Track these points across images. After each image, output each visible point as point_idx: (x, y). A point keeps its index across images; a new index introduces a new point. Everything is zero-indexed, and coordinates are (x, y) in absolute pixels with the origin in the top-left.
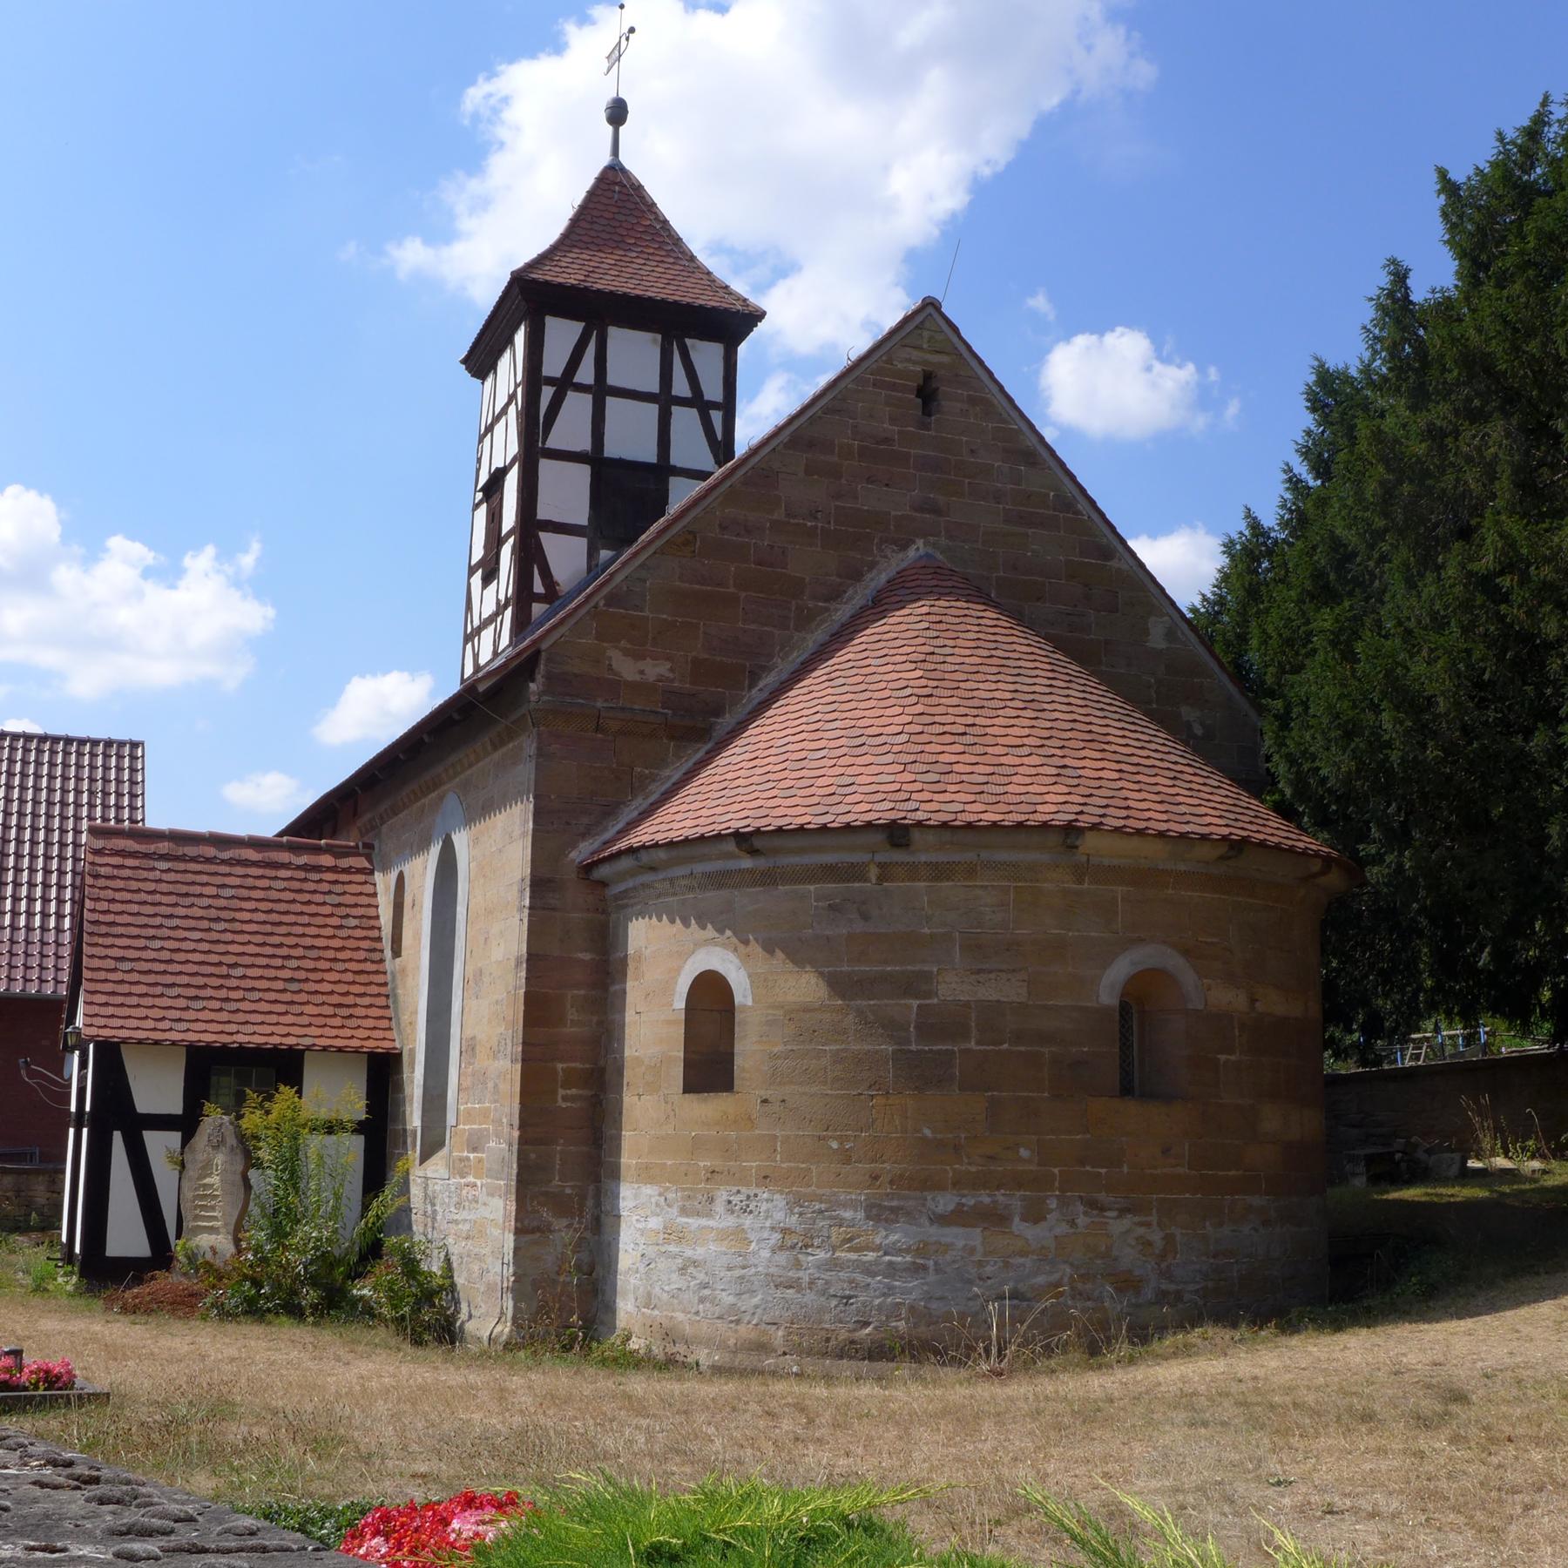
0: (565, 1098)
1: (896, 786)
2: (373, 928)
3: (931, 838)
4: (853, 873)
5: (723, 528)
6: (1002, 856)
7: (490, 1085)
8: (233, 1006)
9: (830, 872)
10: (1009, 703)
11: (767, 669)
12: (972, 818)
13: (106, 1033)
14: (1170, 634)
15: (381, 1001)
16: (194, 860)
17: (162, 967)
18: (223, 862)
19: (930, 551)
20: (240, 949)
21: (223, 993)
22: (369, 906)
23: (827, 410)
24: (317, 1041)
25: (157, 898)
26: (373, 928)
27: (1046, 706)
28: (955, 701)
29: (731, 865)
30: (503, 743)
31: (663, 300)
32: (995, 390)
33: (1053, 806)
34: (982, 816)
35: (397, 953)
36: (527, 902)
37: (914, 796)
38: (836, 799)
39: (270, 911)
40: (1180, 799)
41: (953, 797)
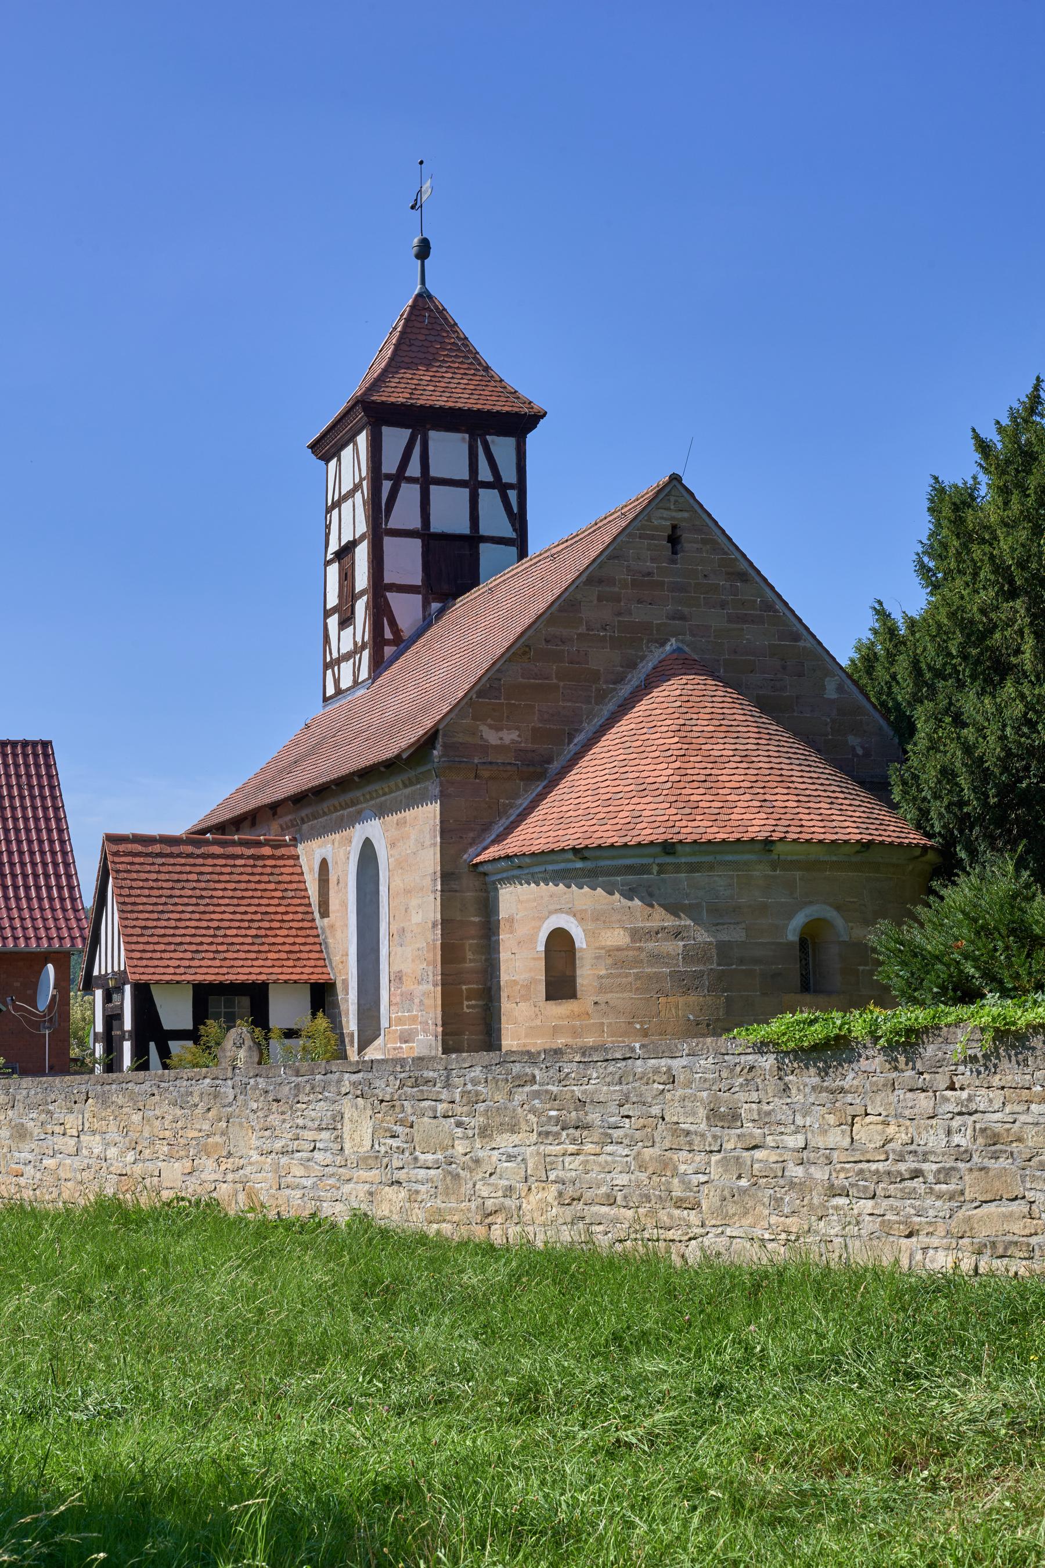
0: (468, 1007)
1: (666, 818)
2: (304, 897)
3: (687, 849)
4: (644, 869)
5: (547, 641)
6: (729, 857)
7: (417, 1001)
8: (222, 956)
9: (630, 869)
10: (732, 759)
11: (579, 731)
12: (711, 837)
13: (314, 977)
14: (840, 688)
15: (317, 948)
16: (179, 856)
17: (171, 932)
18: (198, 856)
19: (681, 645)
20: (220, 916)
21: (213, 948)
22: (300, 882)
23: (610, 558)
24: (280, 977)
25: (160, 884)
26: (304, 897)
27: (754, 759)
28: (699, 758)
29: (570, 866)
30: (411, 784)
31: (469, 409)
32: (719, 532)
33: (758, 827)
34: (717, 836)
35: (325, 913)
36: (439, 888)
37: (677, 824)
38: (631, 826)
39: (235, 889)
40: (834, 817)
41: (700, 824)
